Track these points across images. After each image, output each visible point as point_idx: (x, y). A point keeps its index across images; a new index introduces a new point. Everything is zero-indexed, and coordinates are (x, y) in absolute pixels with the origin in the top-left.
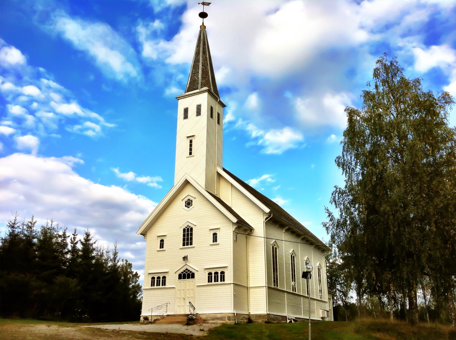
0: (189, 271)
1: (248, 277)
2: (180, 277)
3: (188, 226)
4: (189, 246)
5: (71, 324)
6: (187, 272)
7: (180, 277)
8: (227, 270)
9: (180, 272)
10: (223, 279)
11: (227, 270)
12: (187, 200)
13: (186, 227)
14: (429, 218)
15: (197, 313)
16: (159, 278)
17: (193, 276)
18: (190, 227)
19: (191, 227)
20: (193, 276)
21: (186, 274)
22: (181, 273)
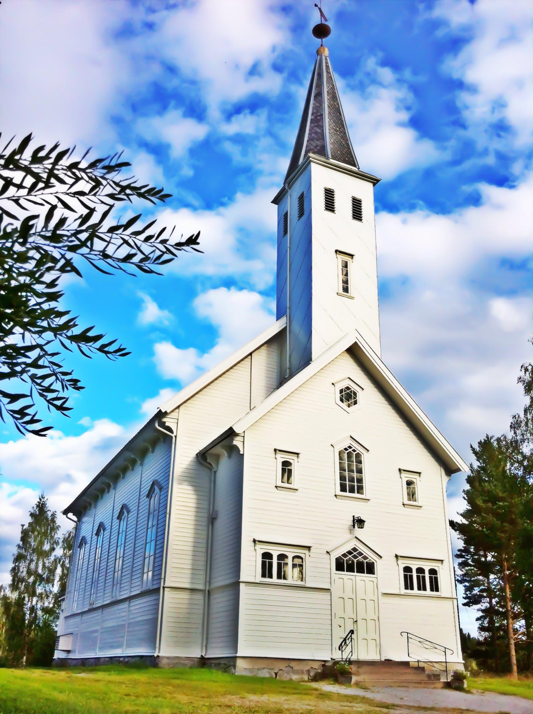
0: (360, 554)
1: (208, 580)
2: (340, 566)
3: (350, 447)
4: (356, 495)
5: (34, 673)
6: (355, 557)
7: (340, 566)
8: (310, 556)
9: (338, 553)
10: (435, 587)
11: (310, 556)
12: (353, 389)
13: (346, 449)
14: (347, 156)
15: (387, 658)
16: (282, 557)
17: (370, 569)
18: (354, 451)
19: (358, 453)
20: (370, 569)
21: (355, 561)
22: (342, 555)
